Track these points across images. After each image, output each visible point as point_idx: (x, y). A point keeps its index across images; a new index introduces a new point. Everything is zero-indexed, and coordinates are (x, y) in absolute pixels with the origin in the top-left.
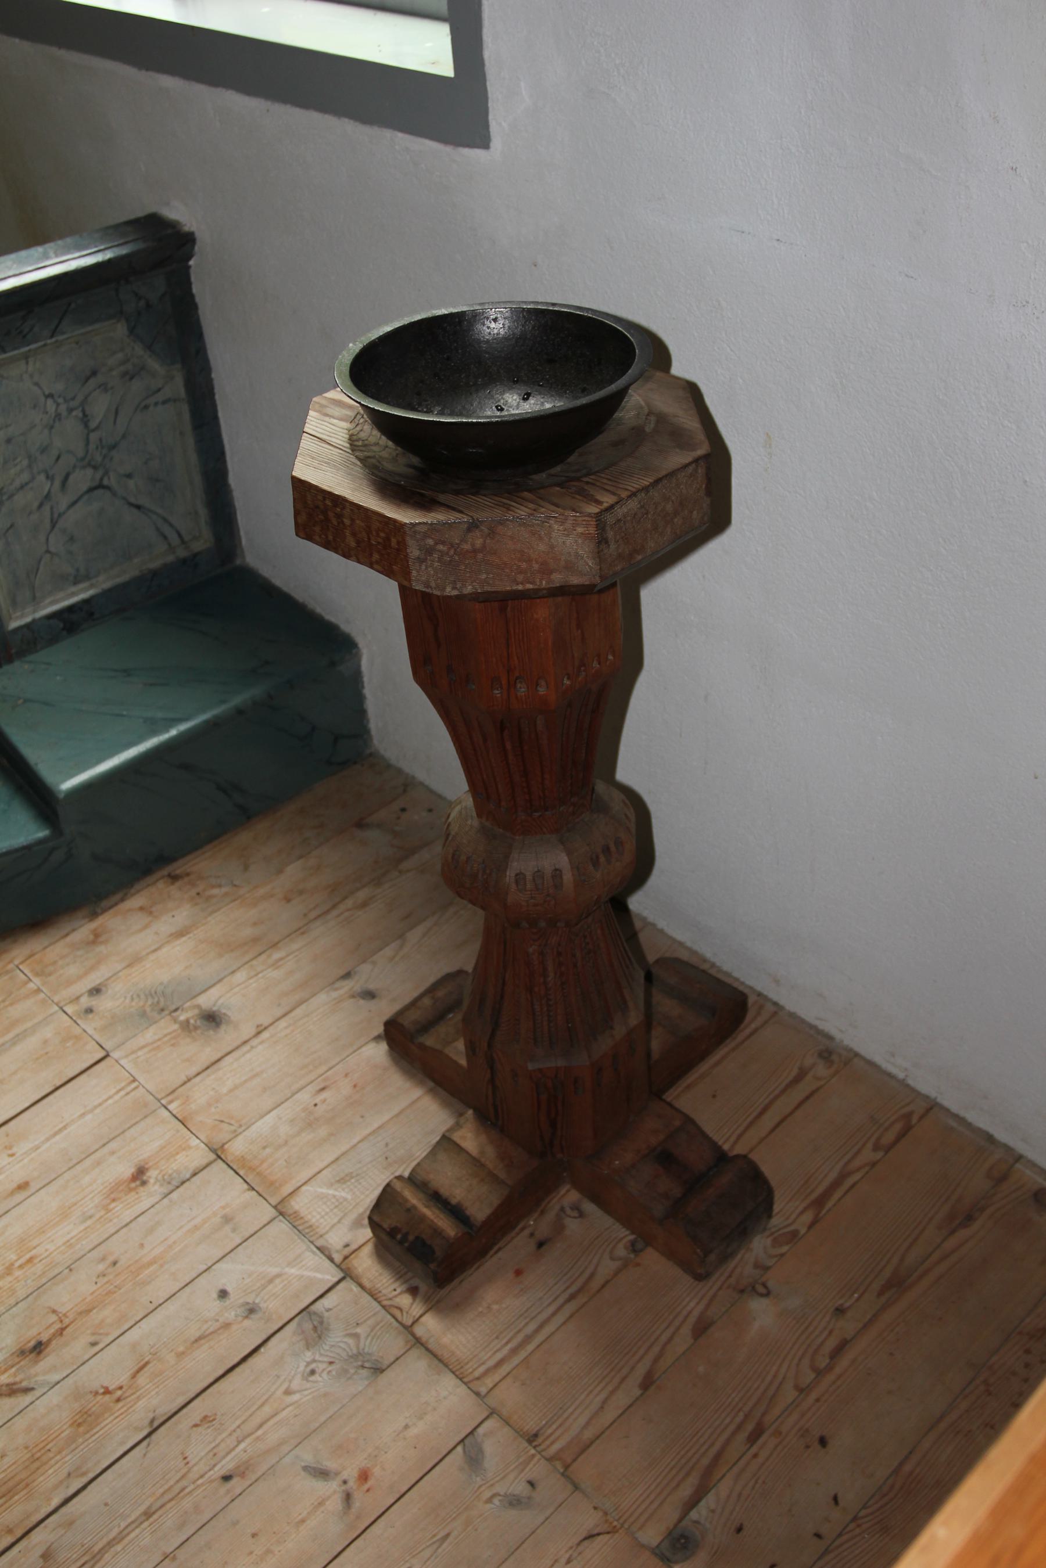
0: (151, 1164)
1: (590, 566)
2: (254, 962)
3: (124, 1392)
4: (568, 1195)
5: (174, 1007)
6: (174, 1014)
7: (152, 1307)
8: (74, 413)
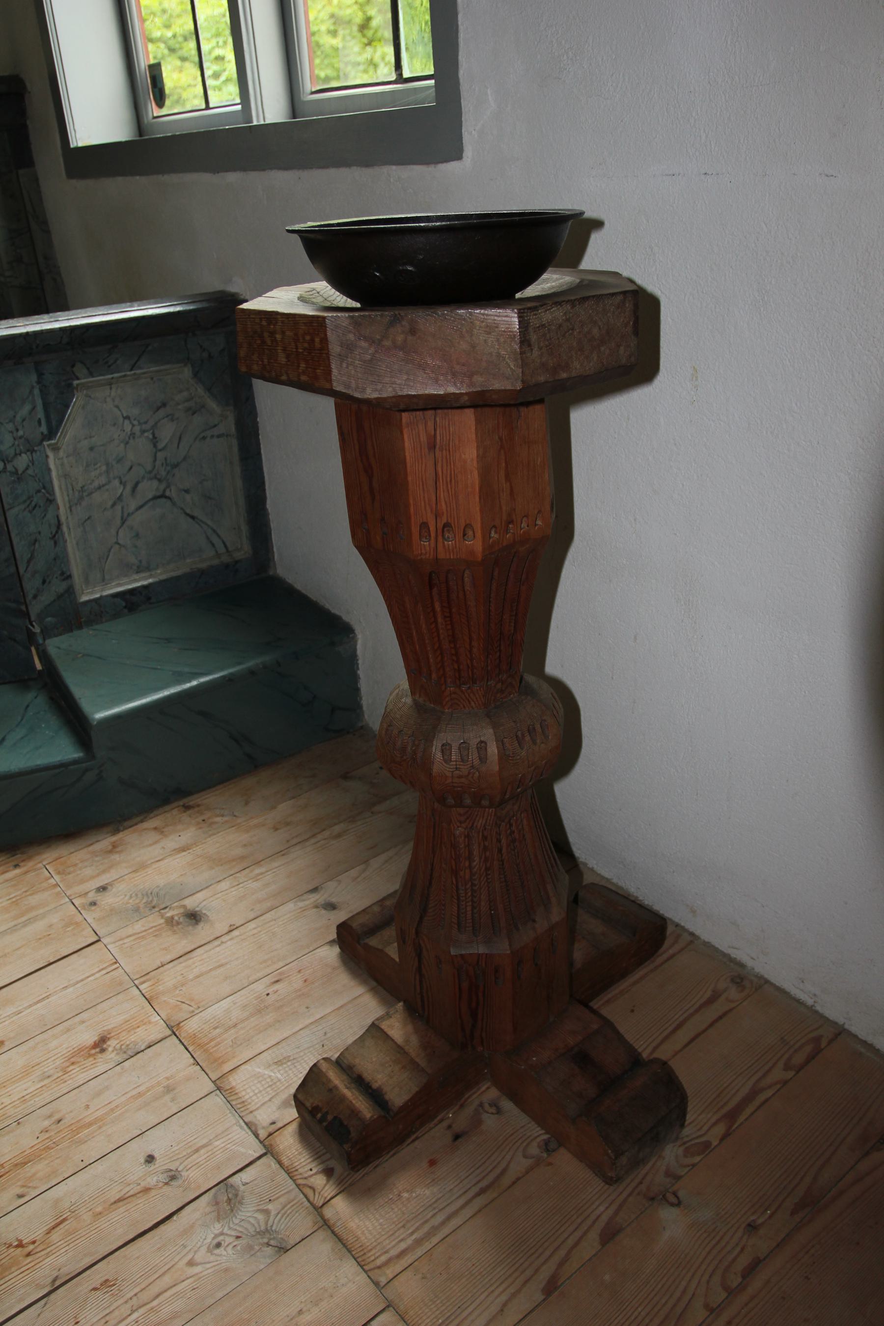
0: (112, 1034)
1: (511, 369)
2: (238, 875)
3: (36, 1247)
4: (488, 1092)
5: (164, 906)
6: (162, 911)
7: (83, 1165)
8: (146, 434)
